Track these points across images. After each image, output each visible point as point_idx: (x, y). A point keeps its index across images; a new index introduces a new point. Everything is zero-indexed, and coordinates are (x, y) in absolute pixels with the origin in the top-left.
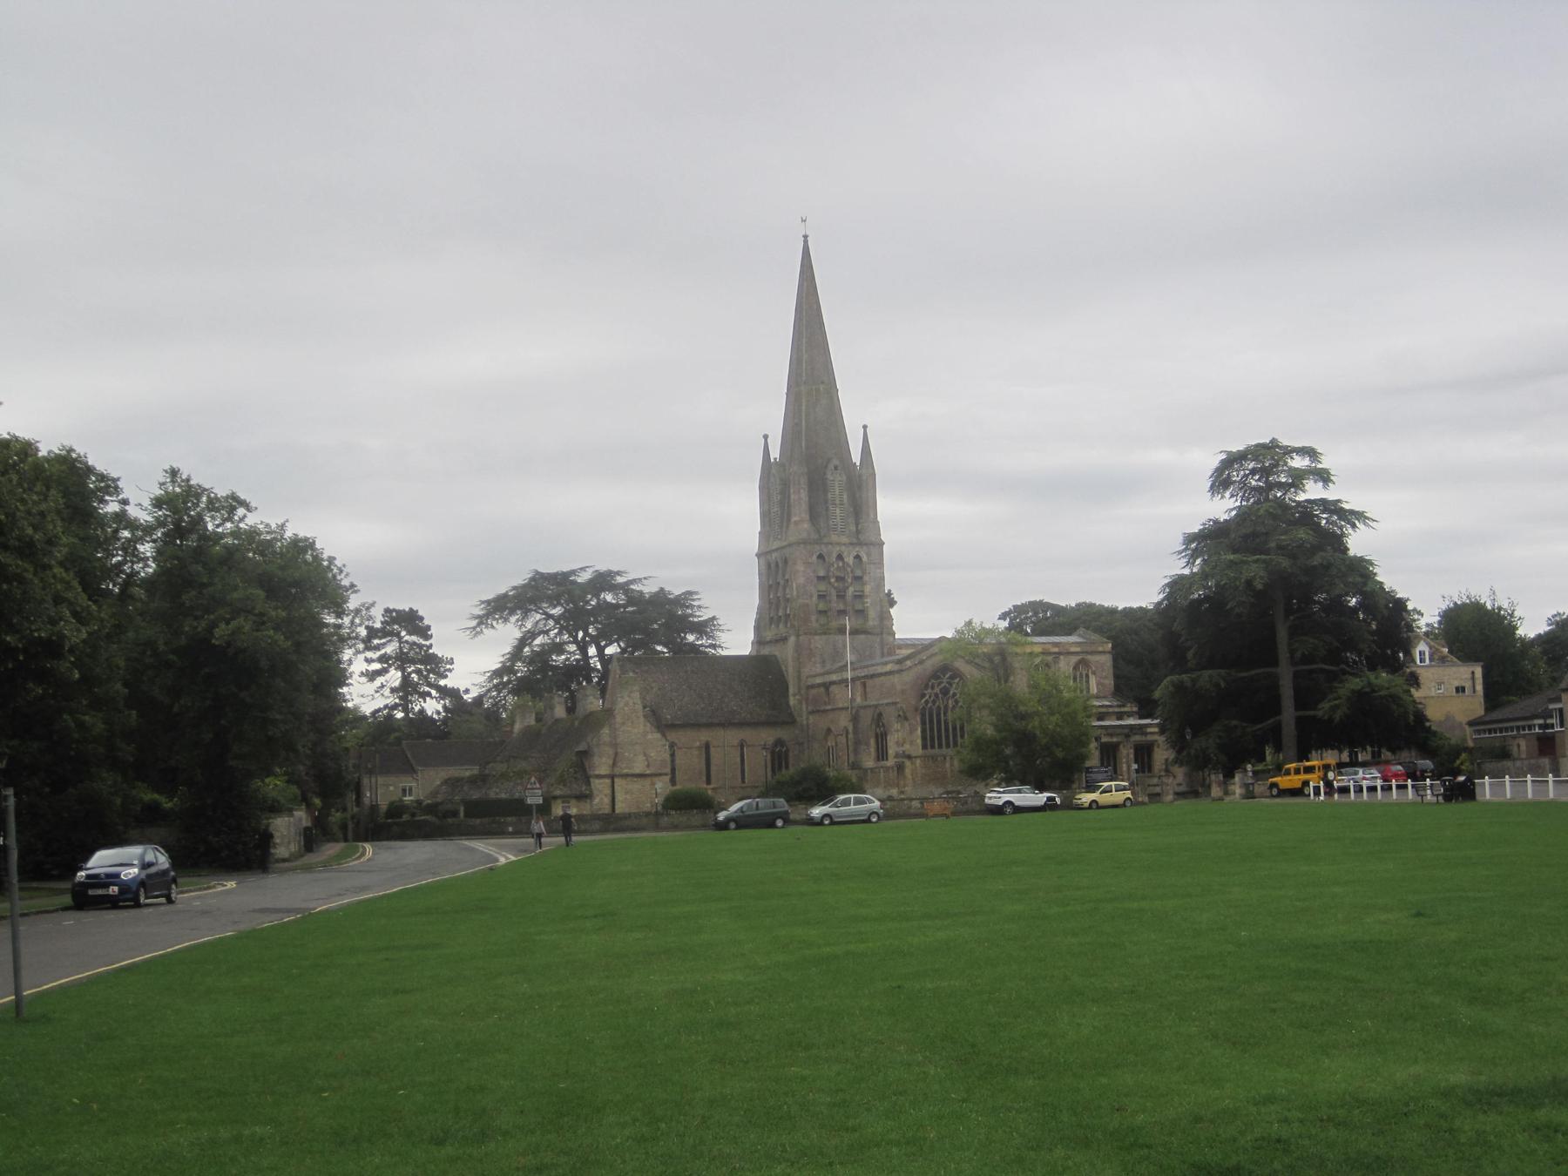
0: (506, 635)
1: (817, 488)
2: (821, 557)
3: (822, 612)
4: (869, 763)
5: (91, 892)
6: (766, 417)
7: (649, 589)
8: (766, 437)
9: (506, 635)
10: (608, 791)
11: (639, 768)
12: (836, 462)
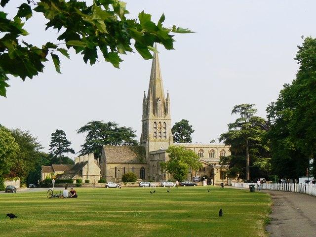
2: (155, 122)
4: (160, 174)
11: (93, 174)
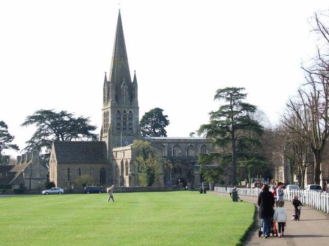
0: (33, 128)
2: (118, 111)
3: (118, 129)
6: (105, 67)
7: (76, 117)
8: (106, 73)
9: (33, 128)
10: (29, 183)
11: (38, 176)
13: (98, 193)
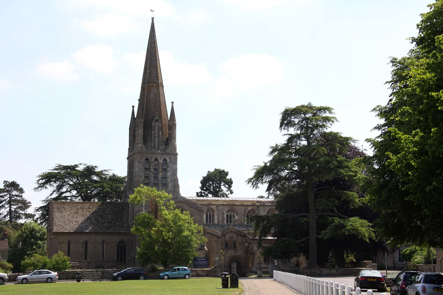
0: (49, 192)
1: (152, 127)
2: (147, 159)
5: (377, 290)
9: (49, 192)
12: (157, 118)
13: (139, 279)
